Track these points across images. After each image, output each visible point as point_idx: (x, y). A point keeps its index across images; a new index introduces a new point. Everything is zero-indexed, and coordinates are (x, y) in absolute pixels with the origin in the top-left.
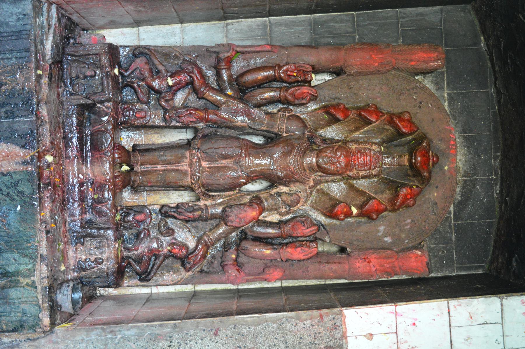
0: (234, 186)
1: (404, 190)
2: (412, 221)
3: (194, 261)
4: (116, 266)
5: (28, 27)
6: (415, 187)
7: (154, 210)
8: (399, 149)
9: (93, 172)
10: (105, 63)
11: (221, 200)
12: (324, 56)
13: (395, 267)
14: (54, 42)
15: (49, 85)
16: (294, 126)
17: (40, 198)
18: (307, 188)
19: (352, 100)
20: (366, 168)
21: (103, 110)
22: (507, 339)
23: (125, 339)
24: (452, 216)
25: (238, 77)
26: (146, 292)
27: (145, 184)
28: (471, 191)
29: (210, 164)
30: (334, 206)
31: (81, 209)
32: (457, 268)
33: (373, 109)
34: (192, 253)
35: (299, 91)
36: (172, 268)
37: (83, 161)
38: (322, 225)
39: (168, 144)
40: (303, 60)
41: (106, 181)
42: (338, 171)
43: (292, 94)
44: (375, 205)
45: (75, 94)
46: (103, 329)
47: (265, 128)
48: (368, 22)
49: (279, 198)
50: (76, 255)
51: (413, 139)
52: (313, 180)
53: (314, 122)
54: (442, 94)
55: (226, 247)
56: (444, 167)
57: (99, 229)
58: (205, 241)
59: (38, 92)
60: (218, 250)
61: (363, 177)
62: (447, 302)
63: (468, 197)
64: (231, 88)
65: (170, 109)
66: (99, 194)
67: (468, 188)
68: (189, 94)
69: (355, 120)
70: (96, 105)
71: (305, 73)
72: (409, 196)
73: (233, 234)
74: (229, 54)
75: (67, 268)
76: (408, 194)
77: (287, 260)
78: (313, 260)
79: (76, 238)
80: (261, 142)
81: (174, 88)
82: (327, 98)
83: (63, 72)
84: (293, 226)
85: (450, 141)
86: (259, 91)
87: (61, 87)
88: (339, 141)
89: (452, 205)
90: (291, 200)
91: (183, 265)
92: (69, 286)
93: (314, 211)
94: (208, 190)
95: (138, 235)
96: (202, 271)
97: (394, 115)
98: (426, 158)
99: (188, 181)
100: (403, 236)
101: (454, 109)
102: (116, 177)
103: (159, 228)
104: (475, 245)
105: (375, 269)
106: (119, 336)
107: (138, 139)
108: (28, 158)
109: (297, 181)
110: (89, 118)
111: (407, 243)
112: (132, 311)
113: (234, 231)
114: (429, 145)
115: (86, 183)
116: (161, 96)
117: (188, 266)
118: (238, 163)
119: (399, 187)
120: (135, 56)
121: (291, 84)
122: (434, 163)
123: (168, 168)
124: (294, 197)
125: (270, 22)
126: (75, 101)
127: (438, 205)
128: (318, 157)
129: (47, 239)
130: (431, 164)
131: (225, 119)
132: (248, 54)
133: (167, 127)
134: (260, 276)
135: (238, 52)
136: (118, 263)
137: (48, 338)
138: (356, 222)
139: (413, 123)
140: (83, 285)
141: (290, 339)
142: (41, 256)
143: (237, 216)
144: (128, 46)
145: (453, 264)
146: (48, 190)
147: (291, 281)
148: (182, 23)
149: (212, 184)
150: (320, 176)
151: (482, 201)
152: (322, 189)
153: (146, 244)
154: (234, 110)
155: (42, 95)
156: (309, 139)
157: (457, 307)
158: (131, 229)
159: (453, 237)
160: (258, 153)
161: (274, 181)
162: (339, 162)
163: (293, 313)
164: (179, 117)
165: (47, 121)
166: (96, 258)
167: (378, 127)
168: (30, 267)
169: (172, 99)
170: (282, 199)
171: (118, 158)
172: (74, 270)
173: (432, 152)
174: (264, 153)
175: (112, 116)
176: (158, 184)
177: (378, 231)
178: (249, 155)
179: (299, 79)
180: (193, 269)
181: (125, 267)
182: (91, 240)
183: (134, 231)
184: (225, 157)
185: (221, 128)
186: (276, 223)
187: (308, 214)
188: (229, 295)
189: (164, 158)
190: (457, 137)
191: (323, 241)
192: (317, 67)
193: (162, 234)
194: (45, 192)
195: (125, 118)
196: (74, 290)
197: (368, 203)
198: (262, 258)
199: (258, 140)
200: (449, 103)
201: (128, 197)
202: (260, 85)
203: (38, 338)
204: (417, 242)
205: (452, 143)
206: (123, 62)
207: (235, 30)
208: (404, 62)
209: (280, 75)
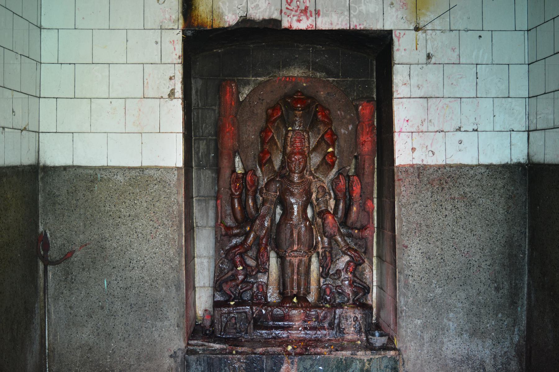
0: (310, 229)
1: (320, 116)
5: (205, 358)
9: (298, 321)
14: (214, 342)
15: (242, 346)
16: (273, 187)
17: (315, 354)
19: (256, 146)
22: (420, 62)
23: (406, 304)
25: (237, 222)
30: (327, 163)
34: (353, 259)
36: (362, 272)
38: (339, 171)
40: (228, 178)
43: (251, 187)
46: (399, 318)
50: (351, 334)
51: (284, 106)
55: (350, 236)
57: (334, 318)
58: (346, 250)
59: (247, 354)
61: (309, 143)
64: (245, 227)
67: (317, 67)
68: (248, 256)
74: (223, 228)
75: (358, 340)
77: (361, 196)
79: (340, 333)
83: (231, 338)
84: (339, 191)
86: (248, 209)
88: (283, 157)
91: (360, 265)
94: (312, 247)
95: (339, 293)
96: (365, 253)
99: (305, 259)
100: (348, 117)
102: (302, 306)
103: (335, 279)
106: (404, 308)
108: (290, 361)
109: (310, 187)
110: (262, 322)
112: (388, 299)
118: (296, 226)
128: (295, 173)
129: (342, 350)
131: (266, 232)
133: (266, 271)
135: (221, 222)
137: (403, 353)
138: (338, 148)
140: (370, 330)
141: (412, 200)
142: (352, 354)
143: (331, 229)
148: (194, 257)
150: (307, 171)
161: (308, 202)
162: (299, 160)
168: (358, 362)
169: (251, 267)
172: (361, 336)
175: (262, 307)
181: (360, 303)
183: (337, 295)
184: (292, 234)
189: (290, 274)
196: (374, 335)
198: (358, 212)
199: (279, 211)
200: (259, 77)
201: (311, 298)
203: (403, 359)
205: (288, 79)
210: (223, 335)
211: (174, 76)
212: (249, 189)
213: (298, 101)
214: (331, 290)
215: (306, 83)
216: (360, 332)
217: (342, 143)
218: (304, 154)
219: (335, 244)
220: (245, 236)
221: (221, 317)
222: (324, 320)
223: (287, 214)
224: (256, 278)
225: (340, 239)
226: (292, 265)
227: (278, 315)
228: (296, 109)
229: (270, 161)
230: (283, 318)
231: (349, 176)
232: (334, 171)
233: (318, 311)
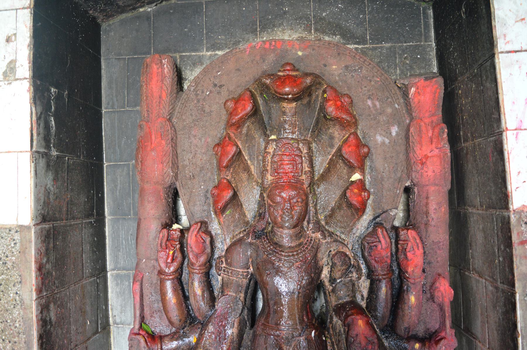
2: (369, 98)
6: (325, 95)
8: (275, 113)
13: (432, 122)
18: (324, 241)
19: (209, 174)
24: (360, 47)
28: (330, 23)
30: (350, 205)
32: (426, 41)
33: (220, 149)
35: (193, 247)
38: (375, 219)
42: (303, 200)
43: (197, 257)
44: (350, 149)
47: (242, 295)
48: (117, 148)
49: (338, 281)
52: (313, 233)
53: (236, 226)
54: (207, 57)
56: (299, 56)
62: (500, 55)
63: (336, 26)
67: (325, 26)
69: (236, 172)
72: (339, 103)
76: (336, 105)
77: (424, 271)
78: (424, 234)
82: (205, 208)
85: (265, 49)
86: (192, 300)
88: (261, 195)
90: (342, 266)
97: (228, 122)
98: (287, 80)
100: (389, 110)
101: (226, 44)
104: (397, 19)
105: (435, 149)
109: (315, 256)
111: (398, 105)
114: (269, 76)
119: (325, 117)
122: (295, 69)
125: (114, 270)
127: (348, 63)
130: (294, 73)
132: (145, 311)
135: (141, 327)
139: (240, 96)
145: (421, 46)
150: (308, 223)
151: (341, 10)
152: (325, 217)
154: (216, 338)
156: (258, 236)
157: (508, 39)
159: (388, 45)
160: (276, 312)
162: (290, 200)
163: (517, 285)
170: (339, 278)
173: (280, 71)
174: (276, 303)
177: (383, 143)
178: (278, 324)
179: (178, 246)
186: (371, 284)
187: (360, 237)
190: (261, 40)
192: (164, 220)
197: (347, 160)
198: (419, 304)
200: (219, 49)
204: (398, 91)
207: (121, 313)
208: (162, 107)
209: (172, 272)
211: (15, 35)
212: (194, 261)
213: (283, 81)
215: (303, 50)
217: (378, 161)
228: (281, 98)
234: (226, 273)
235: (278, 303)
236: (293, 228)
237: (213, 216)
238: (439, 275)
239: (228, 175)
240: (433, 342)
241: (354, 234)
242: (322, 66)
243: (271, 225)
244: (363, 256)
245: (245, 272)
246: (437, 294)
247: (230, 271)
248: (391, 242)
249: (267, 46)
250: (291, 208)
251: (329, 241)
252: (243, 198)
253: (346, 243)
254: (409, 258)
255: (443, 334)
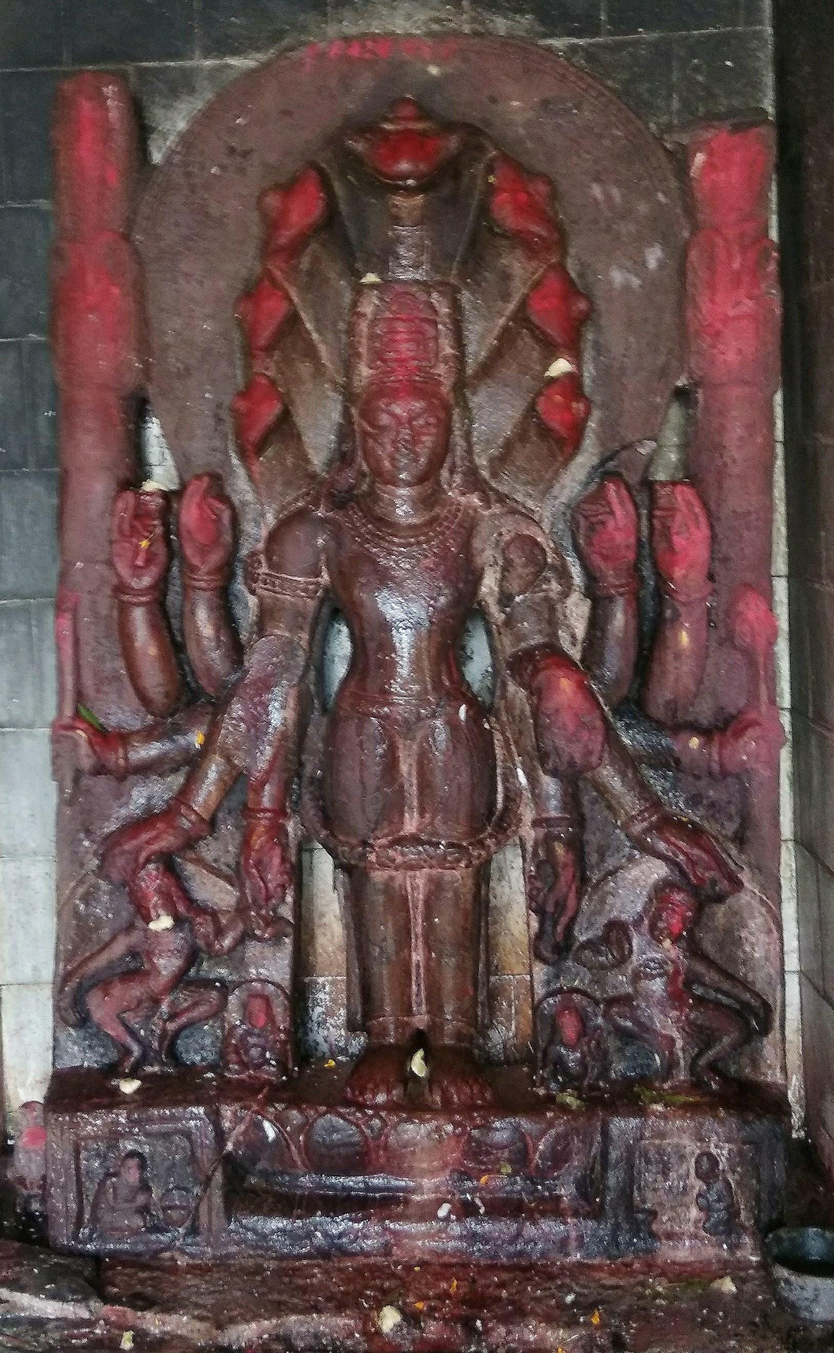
2: (597, 179)
3: (708, 868)
4: (722, 1113)
6: (492, 179)
7: (548, 983)
9: (432, 1173)
10: (105, 1124)
11: (520, 772)
12: (92, 453)
13: (742, 235)
14: (37, 1290)
15: (167, 1307)
18: (486, 513)
20: (431, 332)
21: (244, 1133)
24: (581, 42)
26: (797, 987)
27: (467, 1003)
29: (411, 808)
30: (545, 432)
31: (543, 1214)
37: (396, 1201)
38: (603, 462)
39: (346, 927)
41: (458, 1136)
43: (203, 551)
45: (196, 1218)
47: (305, 636)
49: (518, 599)
51: (342, 174)
52: (463, 494)
55: (665, 761)
58: (647, 831)
60: (674, 787)
61: (459, 342)
65: (245, 924)
66: (498, 1160)
68: (200, 862)
69: (287, 361)
70: (230, 1153)
71: (140, 514)
72: (523, 197)
73: (627, 741)
77: (711, 577)
79: (636, 1233)
80: (345, 630)
81: (181, 908)
82: (217, 443)
84: (605, 558)
85: (349, 60)
86: (192, 652)
87: (173, 1259)
88: (346, 414)
89: (550, 41)
90: (525, 566)
91: (720, 899)
92: (787, 1281)
93: (557, 487)
95: (626, 1036)
96: (740, 840)
99: (458, 875)
100: (643, 208)
102: (446, 1100)
103: (602, 967)
105: (747, 301)
107: (330, 994)
109: (466, 546)
110: (265, 1175)
111: (665, 194)
113: (617, 739)
115: (463, 1192)
116: (204, 948)
117: (724, 885)
118: (409, 727)
119: (490, 229)
120: (83, 1021)
121: (172, 553)
122: (424, 113)
123: (419, 930)
124: (518, 559)
126: (214, 1219)
128: (395, 482)
130: (419, 126)
131: (275, 757)
134: (758, 666)
135: (77, 715)
136: (712, 1108)
144: (55, 1039)
146: (487, 1331)
147: (775, 549)
149: (473, 803)
150: (452, 472)
152: (491, 460)
153: (655, 1011)
155: (195, 1335)
158: (606, 1053)
160: (381, 664)
162: (411, 420)
164: (268, 898)
165: (274, 1321)
166: (698, 1175)
167: (305, 289)
169: (214, 914)
171: (389, 1092)
173: (386, 120)
176: (469, 964)
177: (627, 288)
178: (386, 693)
179: (159, 530)
180: (733, 866)
182: (639, 1188)
183: (612, 1043)
185: (301, 764)
186: (594, 608)
187: (568, 506)
188: (814, 750)
189: (390, 946)
191: (650, 460)
192: (123, 473)
193: (622, 960)
194: (492, 1340)
195: (267, 1062)
197: (538, 328)
198: (702, 653)
199: (342, 645)
200: (235, 52)
202: (174, 645)
204: (664, 160)
206: (102, 1056)
210: (90, 1239)
212: (196, 561)
214: (583, 1019)
216: (728, 1228)
217: (614, 335)
218: (436, 395)
219: (594, 802)
220: (185, 769)
221: (77, 1152)
222: (557, 1166)
223: (363, 679)
224: (240, 964)
225: (616, 784)
226: (399, 902)
227: (333, 1145)
229: (284, 428)
230: (359, 1159)
231: (648, 485)
232: (585, 460)
233: (526, 1124)
234: (270, 587)
235: (387, 646)
236: (417, 484)
237: (235, 461)
238: (748, 586)
239: (268, 368)
240: (729, 733)
241: (556, 498)
242: (485, 100)
243: (367, 480)
244: (577, 548)
245: (312, 584)
246: (741, 628)
247: (277, 582)
248: (639, 516)
249: (355, 52)
250: (413, 437)
251: (497, 511)
252: (302, 419)
253: (536, 518)
254: (677, 548)
255: (753, 715)
